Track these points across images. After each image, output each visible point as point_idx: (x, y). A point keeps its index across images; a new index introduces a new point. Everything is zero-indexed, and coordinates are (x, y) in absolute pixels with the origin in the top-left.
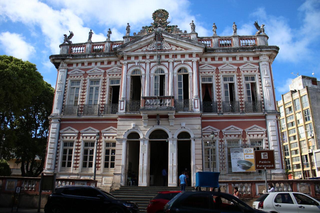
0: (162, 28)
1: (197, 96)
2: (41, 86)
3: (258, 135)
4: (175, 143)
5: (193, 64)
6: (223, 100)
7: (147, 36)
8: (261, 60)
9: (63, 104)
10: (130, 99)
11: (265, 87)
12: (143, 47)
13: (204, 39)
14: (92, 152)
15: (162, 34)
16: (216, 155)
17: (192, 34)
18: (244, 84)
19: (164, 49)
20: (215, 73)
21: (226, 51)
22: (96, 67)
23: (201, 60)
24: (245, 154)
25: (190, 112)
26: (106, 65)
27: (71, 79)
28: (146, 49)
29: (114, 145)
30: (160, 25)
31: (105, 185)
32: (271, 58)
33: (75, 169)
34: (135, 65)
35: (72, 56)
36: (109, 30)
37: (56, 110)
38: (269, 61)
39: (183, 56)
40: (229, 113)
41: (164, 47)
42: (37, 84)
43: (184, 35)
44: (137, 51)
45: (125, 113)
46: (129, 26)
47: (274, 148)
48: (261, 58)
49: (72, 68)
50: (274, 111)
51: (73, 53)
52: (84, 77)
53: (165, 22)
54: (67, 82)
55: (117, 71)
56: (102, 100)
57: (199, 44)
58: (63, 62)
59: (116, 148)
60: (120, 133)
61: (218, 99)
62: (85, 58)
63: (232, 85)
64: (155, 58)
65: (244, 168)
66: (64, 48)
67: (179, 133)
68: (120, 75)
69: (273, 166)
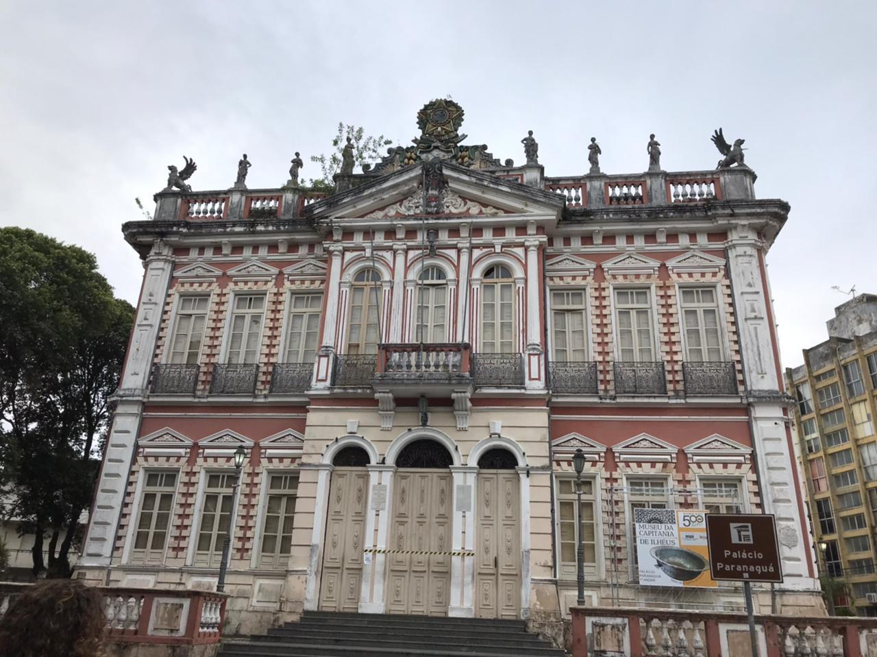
0: (443, 153)
6: (616, 357)
7: (401, 173)
8: (732, 241)
9: (153, 360)
12: (388, 206)
13: (561, 183)
15: (441, 171)
18: (679, 311)
19: (447, 211)
20: (593, 279)
21: (624, 217)
22: (256, 258)
23: (550, 242)
28: (397, 212)
32: (765, 236)
34: (365, 257)
35: (187, 225)
40: (633, 397)
41: (448, 207)
44: (372, 215)
48: (734, 237)
49: (186, 260)
50: (777, 392)
51: (192, 218)
53: (452, 135)
54: (169, 300)
58: (162, 243)
61: (600, 353)
62: (225, 234)
65: (679, 574)
67: (480, 455)
68: (322, 283)
69: (772, 569)
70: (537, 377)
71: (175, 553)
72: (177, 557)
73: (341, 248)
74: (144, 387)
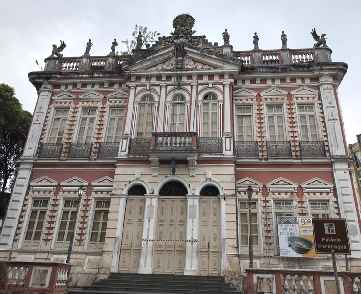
0: (185, 40)
5: (225, 88)
6: (268, 139)
7: (164, 49)
8: (321, 82)
12: (158, 64)
13: (240, 54)
15: (184, 48)
16: (257, 223)
19: (186, 67)
22: (93, 90)
23: (236, 82)
24: (300, 227)
27: (56, 105)
28: (162, 68)
30: (183, 35)
38: (334, 83)
39: (211, 76)
40: (276, 159)
43: (214, 49)
44: (150, 69)
48: (322, 80)
49: (59, 91)
51: (63, 70)
53: (189, 31)
54: (49, 111)
57: (233, 60)
58: (47, 82)
61: (259, 137)
65: (300, 250)
68: (125, 102)
69: (345, 247)
70: (229, 149)
71: (46, 242)
72: (46, 245)
73: (135, 85)
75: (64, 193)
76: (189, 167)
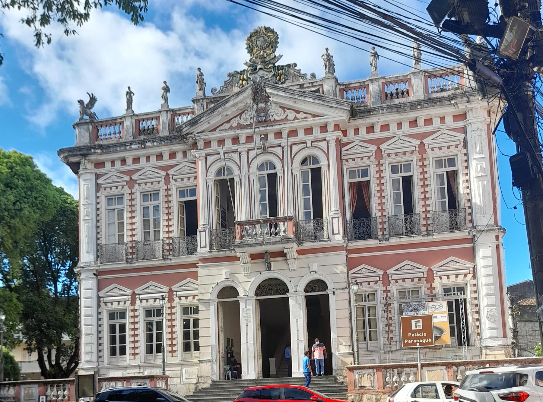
0: (266, 73)
1: (338, 211)
2: (51, 202)
3: (457, 276)
4: (302, 301)
6: (390, 212)
10: (218, 225)
11: (475, 179)
14: (159, 325)
17: (326, 81)
19: (272, 119)
21: (394, 110)
22: (149, 165)
25: (324, 243)
26: (166, 161)
28: (238, 123)
29: (196, 311)
30: (263, 67)
31: (186, 381)
33: (133, 357)
34: (220, 159)
36: (164, 85)
37: (87, 255)
39: (309, 131)
42: (42, 198)
44: (221, 128)
45: (210, 252)
46: (201, 74)
47: (487, 298)
48: (470, 116)
52: (130, 188)
53: (272, 56)
55: (188, 171)
56: (167, 229)
58: (86, 161)
59: (200, 316)
60: (204, 288)
62: (126, 150)
63: (408, 182)
64: (257, 141)
66: (82, 130)
67: (312, 279)
69: (430, 340)
70: (338, 233)
71: (134, 356)
72: (135, 359)
73: (204, 155)
74: (95, 260)
75: (141, 302)
76: (288, 261)
